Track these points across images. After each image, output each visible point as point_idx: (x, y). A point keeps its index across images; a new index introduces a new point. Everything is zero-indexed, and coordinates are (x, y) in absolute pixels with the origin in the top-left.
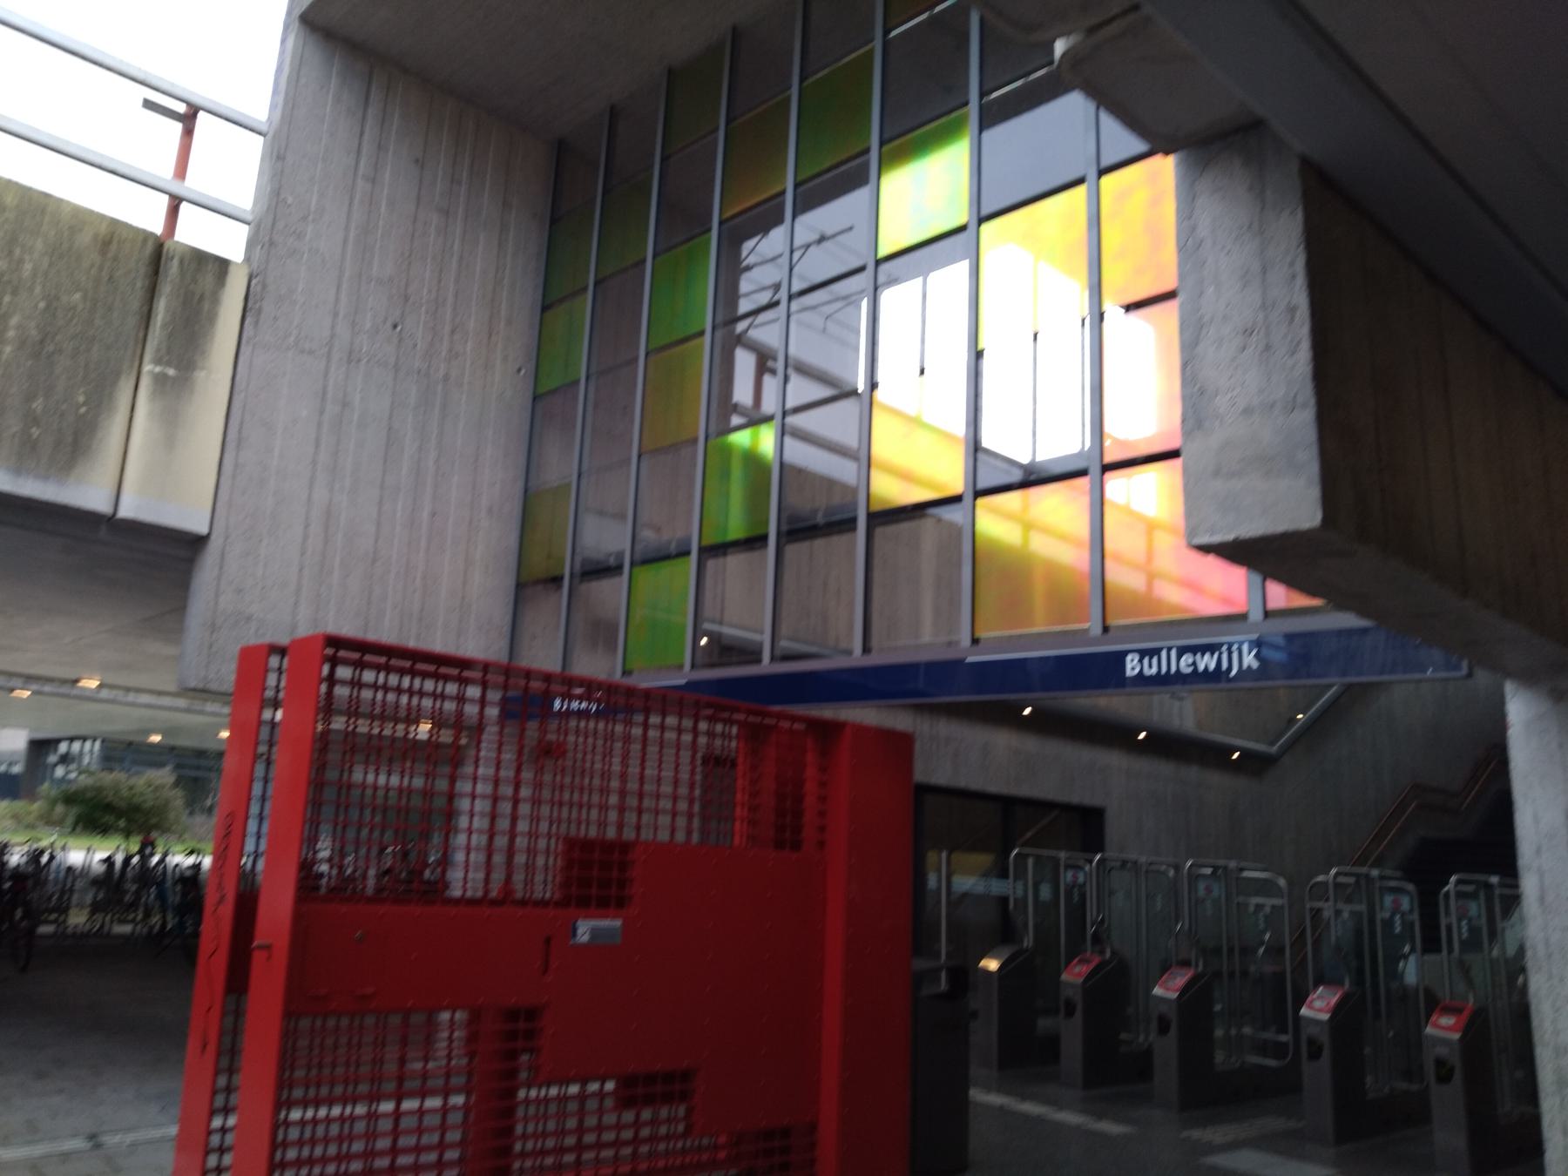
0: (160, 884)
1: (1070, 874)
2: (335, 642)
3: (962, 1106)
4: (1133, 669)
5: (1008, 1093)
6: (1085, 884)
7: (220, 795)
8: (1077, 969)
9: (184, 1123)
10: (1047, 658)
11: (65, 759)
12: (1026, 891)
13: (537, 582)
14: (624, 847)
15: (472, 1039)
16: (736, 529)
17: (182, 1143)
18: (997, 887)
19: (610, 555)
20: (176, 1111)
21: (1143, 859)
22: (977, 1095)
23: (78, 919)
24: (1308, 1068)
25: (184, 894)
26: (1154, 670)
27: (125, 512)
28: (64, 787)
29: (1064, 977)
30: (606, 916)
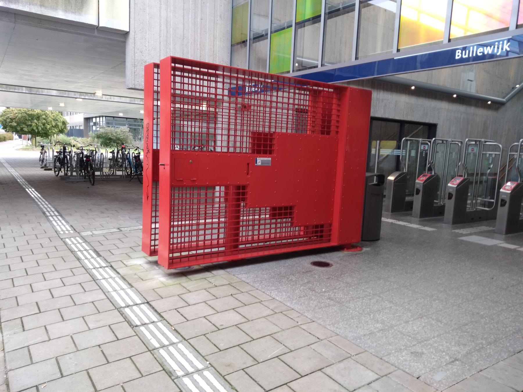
0: (128, 159)
1: (422, 146)
2: (175, 60)
3: (378, 223)
4: (458, 56)
5: (394, 219)
6: (428, 150)
7: (143, 133)
8: (422, 179)
9: (144, 226)
10: (426, 55)
11: (95, 124)
12: (406, 154)
13: (238, 44)
14: (271, 134)
15: (226, 194)
16: (308, 14)
17: (144, 231)
18: (396, 152)
19: (263, 31)
20: (142, 223)
21: (450, 140)
22: (383, 219)
23: (106, 171)
24: (499, 208)
25: (136, 161)
26: (467, 56)
27: (101, 25)
28: (96, 133)
29: (417, 181)
30: (266, 157)
